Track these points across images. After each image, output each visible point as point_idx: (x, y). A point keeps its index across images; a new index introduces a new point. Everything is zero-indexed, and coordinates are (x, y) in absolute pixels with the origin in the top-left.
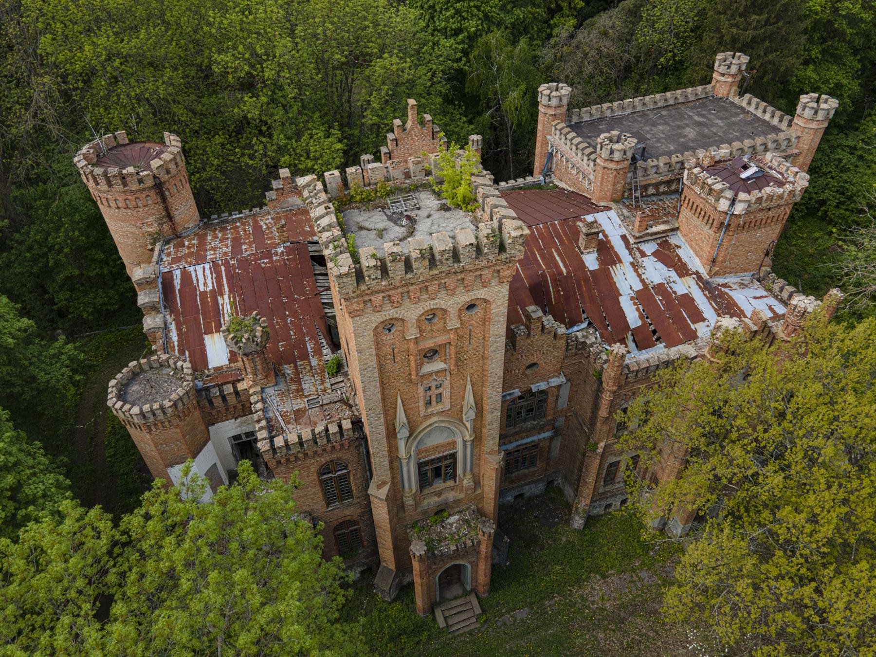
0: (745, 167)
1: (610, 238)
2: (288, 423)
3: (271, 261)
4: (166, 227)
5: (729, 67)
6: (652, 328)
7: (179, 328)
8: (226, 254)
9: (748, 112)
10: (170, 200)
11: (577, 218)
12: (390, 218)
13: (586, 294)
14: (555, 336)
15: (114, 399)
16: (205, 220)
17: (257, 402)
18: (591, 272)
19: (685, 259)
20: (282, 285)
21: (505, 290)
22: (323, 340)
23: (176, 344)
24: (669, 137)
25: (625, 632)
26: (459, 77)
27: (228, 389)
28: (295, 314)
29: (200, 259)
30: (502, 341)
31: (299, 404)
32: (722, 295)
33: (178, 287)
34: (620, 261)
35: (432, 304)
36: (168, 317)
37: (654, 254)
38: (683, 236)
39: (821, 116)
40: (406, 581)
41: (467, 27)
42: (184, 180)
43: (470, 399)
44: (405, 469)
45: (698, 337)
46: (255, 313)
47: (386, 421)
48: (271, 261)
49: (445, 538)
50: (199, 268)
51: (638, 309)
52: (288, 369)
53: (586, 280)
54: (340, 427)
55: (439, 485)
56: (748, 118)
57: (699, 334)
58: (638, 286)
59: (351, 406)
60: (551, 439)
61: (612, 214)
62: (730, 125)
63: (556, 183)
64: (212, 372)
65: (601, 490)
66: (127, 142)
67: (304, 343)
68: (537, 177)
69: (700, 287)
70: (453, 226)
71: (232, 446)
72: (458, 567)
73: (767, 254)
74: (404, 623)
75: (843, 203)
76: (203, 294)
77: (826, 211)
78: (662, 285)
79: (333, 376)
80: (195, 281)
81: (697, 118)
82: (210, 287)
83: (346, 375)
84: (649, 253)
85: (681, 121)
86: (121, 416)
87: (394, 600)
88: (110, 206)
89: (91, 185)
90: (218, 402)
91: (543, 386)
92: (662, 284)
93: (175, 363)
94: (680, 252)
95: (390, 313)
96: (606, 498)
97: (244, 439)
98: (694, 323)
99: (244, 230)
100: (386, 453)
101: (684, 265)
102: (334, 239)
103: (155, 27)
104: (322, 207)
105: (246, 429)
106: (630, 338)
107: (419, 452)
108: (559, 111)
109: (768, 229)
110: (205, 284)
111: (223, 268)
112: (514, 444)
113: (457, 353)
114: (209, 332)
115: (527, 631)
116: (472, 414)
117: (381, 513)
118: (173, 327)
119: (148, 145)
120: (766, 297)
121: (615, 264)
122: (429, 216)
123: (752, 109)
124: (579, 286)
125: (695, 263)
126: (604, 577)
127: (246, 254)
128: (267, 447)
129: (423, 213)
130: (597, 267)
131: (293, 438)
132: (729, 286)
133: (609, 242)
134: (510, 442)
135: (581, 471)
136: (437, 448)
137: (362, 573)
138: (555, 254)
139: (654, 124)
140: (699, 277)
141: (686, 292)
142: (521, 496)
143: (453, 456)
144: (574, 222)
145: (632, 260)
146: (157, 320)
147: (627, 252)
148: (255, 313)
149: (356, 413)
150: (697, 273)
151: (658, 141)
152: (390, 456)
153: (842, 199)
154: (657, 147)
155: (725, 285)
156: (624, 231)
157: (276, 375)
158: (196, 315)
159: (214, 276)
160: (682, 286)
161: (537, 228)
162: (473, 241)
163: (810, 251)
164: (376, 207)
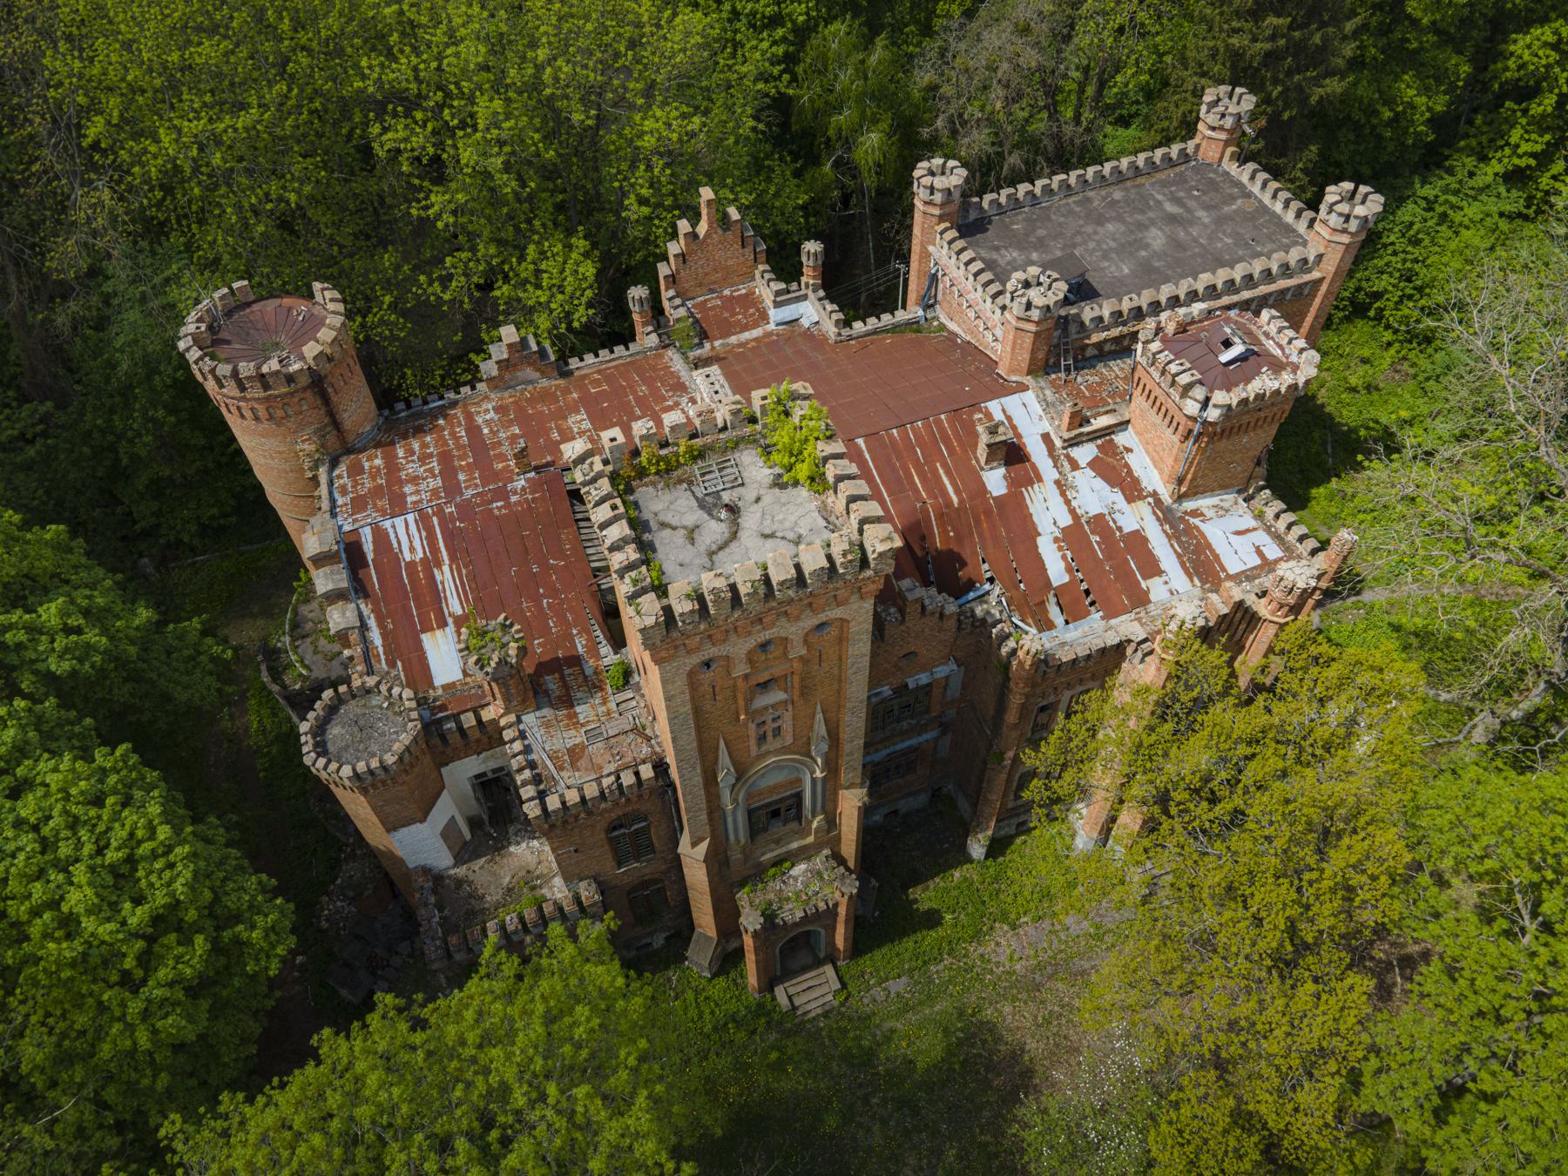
0: (1227, 344)
1: (1024, 440)
2: (560, 768)
3: (508, 505)
4: (332, 439)
5: (1225, 108)
6: (1084, 586)
7: (381, 625)
8: (435, 492)
9: (1249, 195)
10: (335, 399)
11: (975, 407)
12: (702, 505)
13: (987, 534)
14: (942, 615)
15: (313, 755)
16: (386, 412)
17: (512, 741)
19: (1138, 471)
21: (869, 605)
22: (598, 633)
23: (381, 650)
24: (1123, 245)
25: (1042, 1002)
26: (782, 105)
27: (469, 720)
28: (553, 592)
29: (398, 507)
30: (868, 626)
31: (575, 737)
32: (1190, 531)
34: (1040, 480)
35: (767, 635)
36: (362, 606)
37: (1092, 465)
38: (1137, 433)
39: (1353, 226)
40: (734, 945)
41: (789, 15)
42: (352, 363)
43: (820, 728)
44: (730, 819)
45: (1149, 602)
46: (502, 616)
47: (705, 772)
48: (508, 505)
49: (788, 899)
50: (399, 521)
51: (1064, 557)
53: (988, 512)
54: (637, 774)
55: (778, 829)
56: (1250, 206)
57: (1152, 597)
58: (1066, 521)
59: (649, 739)
60: (936, 739)
61: (1029, 397)
62: (1220, 221)
63: (943, 319)
64: (440, 692)
65: (1010, 805)
66: (252, 298)
67: (571, 638)
68: (914, 311)
69: (1158, 519)
70: (793, 518)
71: (473, 786)
72: (808, 933)
73: (1258, 464)
74: (732, 1007)
75: (1410, 297)
76: (411, 565)
77: (1382, 310)
78: (1100, 517)
79: (619, 690)
80: (395, 545)
81: (1170, 208)
82: (420, 555)
83: (638, 688)
84: (1083, 463)
85: (1143, 212)
86: (323, 775)
87: (715, 976)
88: (242, 416)
89: (210, 386)
90: (455, 739)
91: (924, 679)
93: (389, 690)
94: (1131, 459)
95: (711, 651)
96: (1018, 815)
97: (490, 775)
98: (1145, 578)
99: (453, 434)
100: (704, 806)
101: (1136, 481)
102: (631, 567)
103: (270, 84)
104: (607, 505)
105: (493, 764)
106: (1053, 600)
107: (749, 796)
108: (948, 210)
109: (1259, 431)
110: (412, 549)
111: (435, 519)
112: (885, 752)
113: (802, 679)
114: (428, 628)
115: (906, 1008)
116: (824, 747)
117: (696, 874)
118: (372, 623)
119: (287, 301)
120: (1255, 529)
121: (1032, 484)
122: (758, 500)
123: (1256, 189)
124: (978, 521)
125: (1153, 478)
126: (1014, 927)
127: (469, 493)
128: (538, 812)
129: (749, 494)
130: (1004, 491)
131: (572, 797)
132: (1202, 514)
134: (877, 750)
135: (981, 781)
136: (773, 789)
137: (667, 939)
138: (941, 471)
139: (1100, 221)
140: (1158, 502)
141: (1136, 527)
142: (895, 812)
143: (799, 797)
144: (971, 414)
145: (1057, 476)
146: (348, 614)
147: (1050, 462)
148: (502, 616)
149: (658, 749)
150: (1155, 494)
151: (1105, 256)
152: (709, 807)
153: (1408, 291)
154: (1103, 269)
155: (1195, 513)
156: (1046, 426)
157: (536, 693)
158: (407, 606)
159: (424, 534)
160: (1134, 518)
162: (825, 564)
163: (1466, 69)
164: (680, 481)
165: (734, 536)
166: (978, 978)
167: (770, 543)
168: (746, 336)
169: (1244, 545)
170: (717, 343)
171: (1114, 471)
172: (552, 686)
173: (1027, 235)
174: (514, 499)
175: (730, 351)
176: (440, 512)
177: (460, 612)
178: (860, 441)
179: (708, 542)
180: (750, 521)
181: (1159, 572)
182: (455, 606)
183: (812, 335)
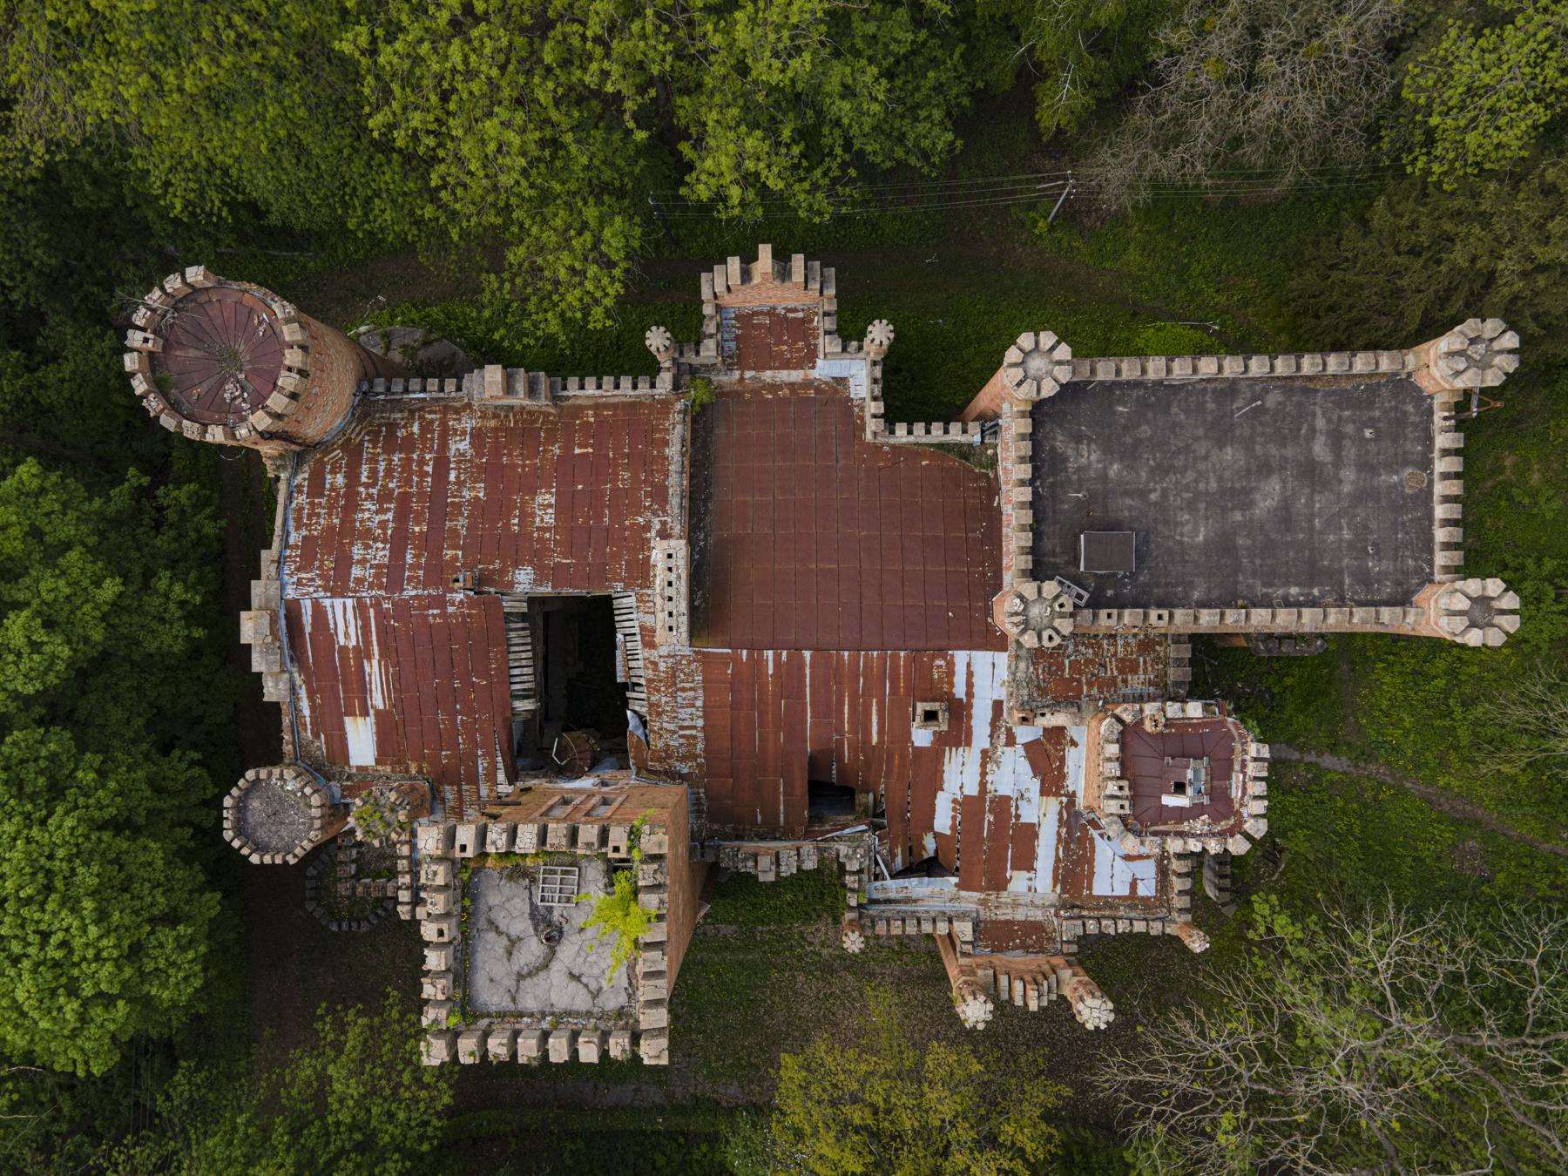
0: (1180, 788)
1: (974, 701)
3: (444, 615)
7: (311, 698)
13: (896, 770)
18: (915, 749)
20: (456, 658)
28: (468, 710)
33: (308, 629)
34: (969, 743)
37: (1027, 746)
48: (444, 615)
50: (338, 602)
51: (954, 818)
52: (449, 792)
53: (903, 757)
57: (1011, 887)
58: (972, 790)
76: (344, 649)
82: (353, 642)
92: (1009, 798)
110: (347, 634)
118: (303, 693)
121: (958, 745)
123: (1441, 465)
133: (970, 705)
141: (1035, 821)
144: (933, 658)
145: (987, 746)
146: (281, 686)
150: (1072, 797)
160: (1041, 813)
161: (866, 656)
165: (545, 966)
166: (791, 948)
167: (574, 984)
168: (785, 376)
169: (1124, 872)
170: (748, 374)
171: (1047, 760)
172: (449, 796)
173: (1125, 428)
174: (450, 609)
175: (756, 393)
176: (377, 605)
177: (381, 707)
178: (807, 654)
179: (522, 962)
180: (567, 952)
181: (1031, 868)
182: (378, 700)
183: (850, 409)
